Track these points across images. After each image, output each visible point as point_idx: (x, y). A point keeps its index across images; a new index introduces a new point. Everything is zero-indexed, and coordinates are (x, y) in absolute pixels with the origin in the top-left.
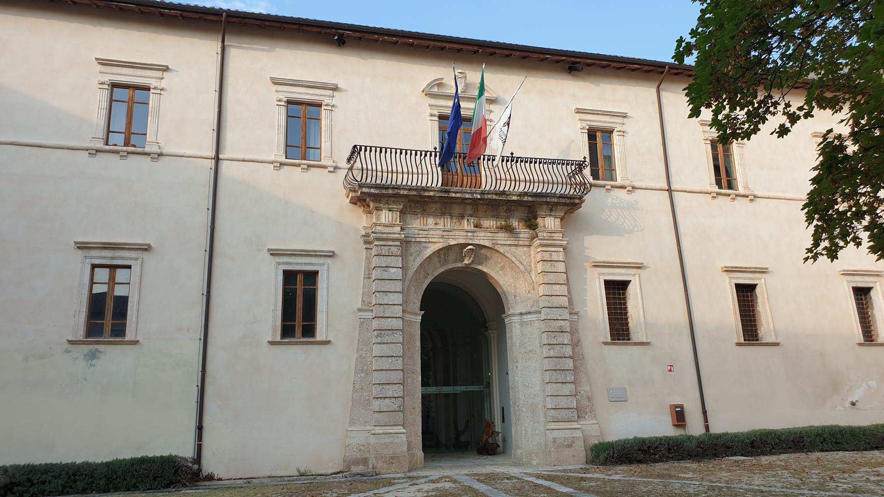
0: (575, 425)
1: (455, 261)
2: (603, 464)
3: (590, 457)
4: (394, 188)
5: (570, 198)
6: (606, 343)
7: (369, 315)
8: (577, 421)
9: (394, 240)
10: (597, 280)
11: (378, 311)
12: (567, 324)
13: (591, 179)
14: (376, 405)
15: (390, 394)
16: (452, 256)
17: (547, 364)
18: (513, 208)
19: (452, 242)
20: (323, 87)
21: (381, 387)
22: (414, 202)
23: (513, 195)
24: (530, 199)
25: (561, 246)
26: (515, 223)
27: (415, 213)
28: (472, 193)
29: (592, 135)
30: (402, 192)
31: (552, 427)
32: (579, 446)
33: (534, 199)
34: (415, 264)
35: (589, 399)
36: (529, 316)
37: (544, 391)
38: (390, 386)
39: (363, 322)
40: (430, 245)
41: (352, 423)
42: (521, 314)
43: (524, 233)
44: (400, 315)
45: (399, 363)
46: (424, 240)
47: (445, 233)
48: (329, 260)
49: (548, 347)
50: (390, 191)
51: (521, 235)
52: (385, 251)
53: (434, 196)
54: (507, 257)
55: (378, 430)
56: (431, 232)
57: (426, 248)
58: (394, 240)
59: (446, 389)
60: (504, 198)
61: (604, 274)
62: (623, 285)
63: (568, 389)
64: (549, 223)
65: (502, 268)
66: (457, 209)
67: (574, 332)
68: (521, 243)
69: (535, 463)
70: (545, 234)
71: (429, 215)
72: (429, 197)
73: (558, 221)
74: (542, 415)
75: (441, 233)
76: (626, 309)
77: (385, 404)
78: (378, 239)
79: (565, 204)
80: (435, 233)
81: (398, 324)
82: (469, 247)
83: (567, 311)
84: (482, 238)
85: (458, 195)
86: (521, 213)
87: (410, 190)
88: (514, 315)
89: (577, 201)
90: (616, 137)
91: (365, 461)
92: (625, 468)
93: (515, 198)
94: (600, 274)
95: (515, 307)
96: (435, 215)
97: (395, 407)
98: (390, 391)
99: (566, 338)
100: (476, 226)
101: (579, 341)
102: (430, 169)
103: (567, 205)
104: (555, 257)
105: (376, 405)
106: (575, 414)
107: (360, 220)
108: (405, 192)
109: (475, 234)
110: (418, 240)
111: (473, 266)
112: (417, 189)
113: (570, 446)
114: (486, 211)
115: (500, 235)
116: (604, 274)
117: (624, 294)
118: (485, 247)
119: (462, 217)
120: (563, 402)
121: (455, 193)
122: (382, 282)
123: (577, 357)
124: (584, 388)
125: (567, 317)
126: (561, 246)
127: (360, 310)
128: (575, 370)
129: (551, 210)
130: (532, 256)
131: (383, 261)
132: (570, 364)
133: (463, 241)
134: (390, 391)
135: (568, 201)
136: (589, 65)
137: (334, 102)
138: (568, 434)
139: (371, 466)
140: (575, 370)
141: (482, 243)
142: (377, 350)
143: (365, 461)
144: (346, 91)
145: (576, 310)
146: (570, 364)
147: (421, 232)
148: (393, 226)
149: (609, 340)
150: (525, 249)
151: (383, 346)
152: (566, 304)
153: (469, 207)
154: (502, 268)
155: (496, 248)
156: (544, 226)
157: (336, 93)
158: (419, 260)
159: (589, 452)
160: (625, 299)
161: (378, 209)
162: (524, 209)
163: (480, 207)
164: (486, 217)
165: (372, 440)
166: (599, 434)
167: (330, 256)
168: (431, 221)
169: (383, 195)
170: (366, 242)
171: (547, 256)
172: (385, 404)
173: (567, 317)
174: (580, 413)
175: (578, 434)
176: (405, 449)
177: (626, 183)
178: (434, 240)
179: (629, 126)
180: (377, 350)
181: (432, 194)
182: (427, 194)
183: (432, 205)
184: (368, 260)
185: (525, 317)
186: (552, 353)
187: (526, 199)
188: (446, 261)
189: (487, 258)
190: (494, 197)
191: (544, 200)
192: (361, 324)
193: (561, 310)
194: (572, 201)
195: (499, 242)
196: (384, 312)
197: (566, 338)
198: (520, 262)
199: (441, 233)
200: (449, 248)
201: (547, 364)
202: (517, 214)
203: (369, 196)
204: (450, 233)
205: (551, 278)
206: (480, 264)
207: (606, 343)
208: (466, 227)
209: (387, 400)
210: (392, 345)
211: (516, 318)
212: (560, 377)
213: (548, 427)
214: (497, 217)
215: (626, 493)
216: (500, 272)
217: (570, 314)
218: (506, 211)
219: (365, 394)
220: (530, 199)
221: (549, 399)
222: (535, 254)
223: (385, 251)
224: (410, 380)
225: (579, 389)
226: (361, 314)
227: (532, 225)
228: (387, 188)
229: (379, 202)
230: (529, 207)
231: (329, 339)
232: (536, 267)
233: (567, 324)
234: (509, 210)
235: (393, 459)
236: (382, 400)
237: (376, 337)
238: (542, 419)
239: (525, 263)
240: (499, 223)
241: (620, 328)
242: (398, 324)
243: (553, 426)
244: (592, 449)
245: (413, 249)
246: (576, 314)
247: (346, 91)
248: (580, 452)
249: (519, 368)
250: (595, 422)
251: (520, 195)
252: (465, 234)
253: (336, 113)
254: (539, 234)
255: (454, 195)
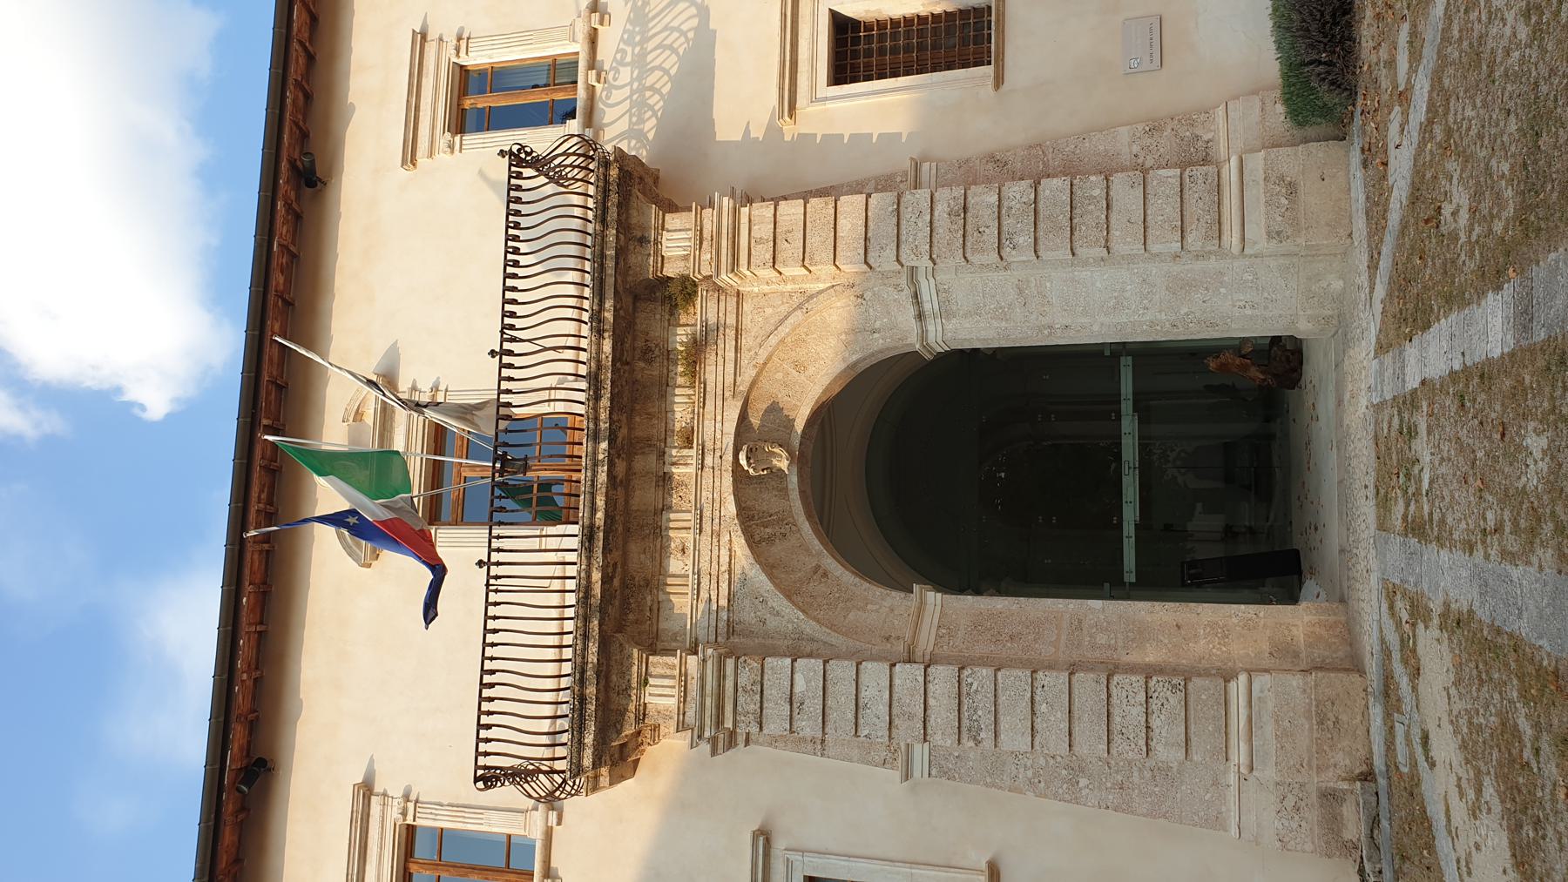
0: (1231, 172)
1: (784, 492)
2: (1352, 94)
3: (1324, 128)
4: (582, 682)
5: (605, 192)
6: (999, 80)
7: (920, 752)
8: (1219, 166)
9: (721, 676)
10: (830, 105)
11: (908, 730)
12: (943, 195)
13: (573, 126)
14: (1167, 752)
15: (1137, 712)
16: (768, 502)
17: (1054, 249)
18: (640, 344)
19: (730, 508)
20: (362, 821)
21: (1117, 738)
22: (621, 613)
23: (599, 350)
24: (609, 304)
25: (735, 213)
26: (681, 337)
27: (658, 608)
28: (595, 464)
29: (461, 122)
30: (593, 658)
31: (1236, 240)
32: (1292, 160)
33: (610, 293)
34: (785, 615)
35: (1154, 129)
36: (925, 296)
37: (1130, 259)
38: (1116, 711)
39: (941, 768)
40: (737, 570)
41: (1216, 822)
42: (920, 316)
43: (706, 310)
44: (918, 670)
45: (1053, 681)
46: (724, 586)
47: (707, 527)
48: (779, 845)
49: (1006, 251)
50: (591, 690)
51: (712, 320)
52: (749, 704)
53: (604, 569)
54: (769, 358)
55: (1239, 754)
56: (704, 565)
57: (744, 580)
58: (721, 676)
59: (1127, 407)
60: (607, 377)
61: (813, 87)
62: (842, 27)
63: (1126, 193)
64: (676, 245)
65: (799, 366)
66: (644, 496)
67: (967, 174)
68: (731, 320)
69: (1338, 285)
70: (706, 257)
71: (661, 570)
72: (606, 580)
73: (673, 220)
74: (1199, 265)
75: (705, 539)
76: (908, 21)
77: (1167, 728)
78: (719, 721)
79: (623, 205)
80: (705, 555)
81: (943, 676)
82: (743, 462)
83: (907, 197)
84: (720, 427)
85: (600, 502)
86: (651, 320)
87: (586, 637)
88: (923, 334)
89: (614, 172)
90: (476, 59)
91: (1330, 798)
92: (1366, 32)
93: (607, 346)
94: (814, 100)
95: (903, 331)
96: (662, 552)
97: (1175, 700)
98: (1129, 713)
99: (984, 199)
100: (688, 443)
101: (992, 158)
102: (552, 557)
103: (629, 193)
104: (764, 230)
105: (1167, 752)
106: (1198, 171)
107: (667, 755)
108: (593, 648)
109: (709, 445)
110: (723, 602)
111: (796, 442)
112: (584, 618)
113: (1292, 189)
114: (650, 416)
115: (710, 378)
116: (813, 87)
117: (868, 27)
118: (743, 417)
119: (665, 480)
120: (1164, 208)
121: (593, 510)
122: (832, 716)
123: (1035, 165)
124: (1124, 143)
125: (923, 194)
126: (735, 213)
127: (907, 776)
128: (1071, 171)
129: (643, 240)
130: (766, 288)
131: (777, 711)
132: (1053, 182)
133: (728, 480)
134: (1129, 713)
135: (614, 198)
136: (304, 136)
137: (396, 792)
138: (1256, 193)
139: (1345, 786)
140: (1071, 171)
141: (731, 427)
142: (1014, 738)
143: (1330, 798)
144: (372, 761)
145: (907, 165)
146: (1055, 188)
147: (704, 595)
148: (684, 676)
149: (988, 70)
150: (747, 307)
151: (1003, 726)
152: (890, 197)
153: (639, 463)
154: (799, 366)
155: (743, 388)
156: (685, 258)
157: (378, 789)
158: (779, 602)
159: (1310, 131)
160: (881, 24)
161: (642, 715)
162: (639, 314)
163: (638, 433)
164: (666, 413)
165: (1268, 773)
166: (1256, 100)
167: (768, 841)
168: (675, 565)
169: (604, 705)
170: (731, 742)
171: (763, 253)
172: (1167, 728)
173: (923, 194)
174: (1197, 158)
175: (1256, 162)
176: (1296, 681)
177: (581, 31)
178: (725, 559)
179: (444, 26)
180: (1014, 738)
181: (596, 576)
182: (597, 590)
183: (633, 565)
184: (774, 741)
185: (927, 307)
186: (1025, 240)
187: (609, 316)
188: (785, 519)
189: (774, 409)
190: (605, 402)
191: (610, 264)
192: (946, 774)
193: (907, 214)
194: (614, 187)
195: (729, 379)
196: (911, 717)
197: (984, 199)
198: (781, 322)
199: (705, 539)
200: (746, 517)
201: (1054, 249)
202: (656, 332)
203: (604, 733)
204: (707, 514)
205: (819, 240)
206: (790, 423)
207: (999, 80)
208: (691, 470)
209: (1155, 722)
210: (1002, 699)
211: (931, 328)
212: (1092, 215)
213: (1236, 249)
214: (664, 387)
215: (1538, 121)
216: (811, 370)
217: (917, 185)
218: (650, 362)
219: (1136, 778)
220: (609, 304)
221: (1154, 248)
222: (757, 281)
223: (749, 704)
224: (1102, 639)
225: (1126, 158)
226: (917, 774)
227: (687, 289)
228: (582, 700)
229: (622, 712)
230: (636, 298)
231: (984, 866)
232: (794, 279)
233: (943, 195)
234: (647, 354)
235: (1324, 719)
236: (1155, 734)
237: (978, 742)
238: (1213, 264)
239: (784, 309)
240: (680, 380)
241: (957, 42)
242: (943, 676)
243: (1232, 238)
244: (1300, 125)
245: (747, 615)
246: (917, 167)
247: (372, 761)
248: (1309, 160)
249: (1068, 321)
250: (1221, 111)
251: (599, 332)
252: (708, 472)
253: (422, 790)
254: (706, 271)
255: (600, 515)
